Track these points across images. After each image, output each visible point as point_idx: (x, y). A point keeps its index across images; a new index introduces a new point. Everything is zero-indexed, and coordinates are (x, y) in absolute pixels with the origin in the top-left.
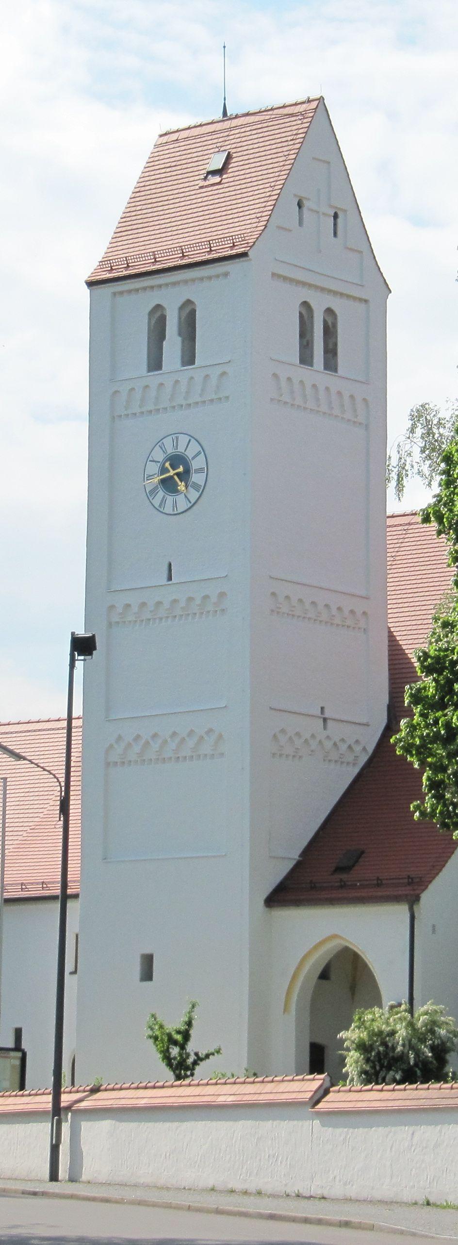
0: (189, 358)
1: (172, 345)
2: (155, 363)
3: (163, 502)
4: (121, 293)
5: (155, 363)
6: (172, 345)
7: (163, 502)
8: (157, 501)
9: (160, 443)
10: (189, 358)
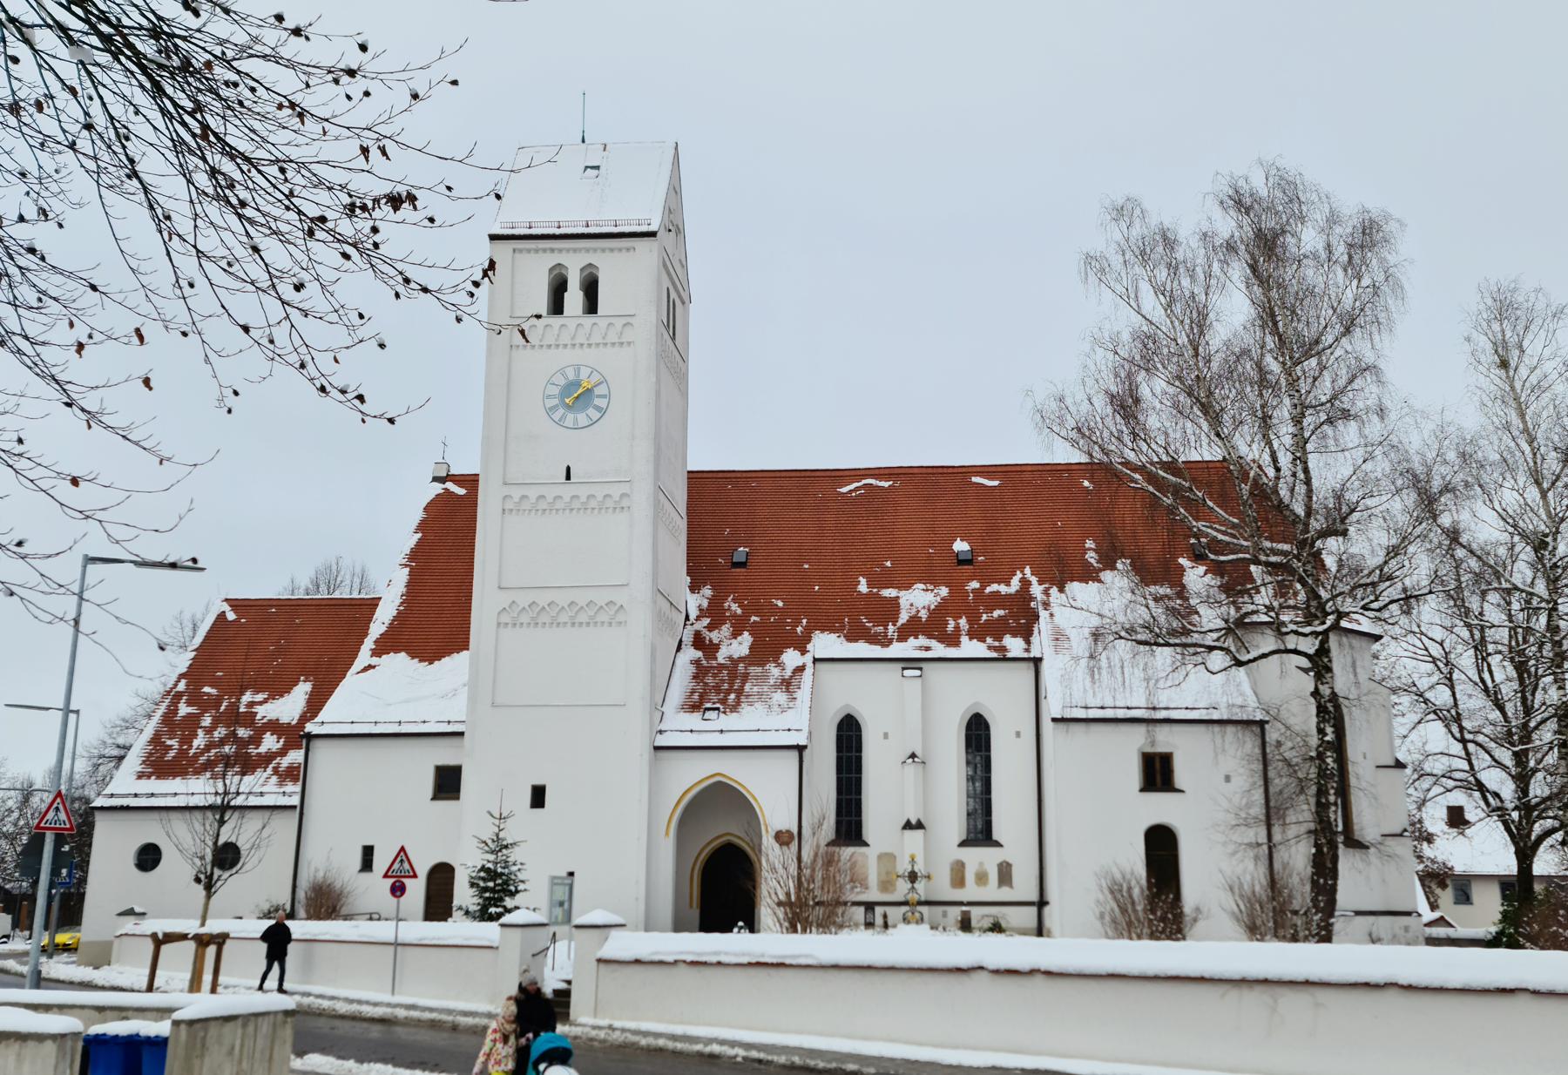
0: (591, 306)
1: (574, 298)
2: (557, 307)
3: (563, 418)
4: (521, 251)
5: (557, 307)
6: (574, 298)
7: (563, 418)
8: (557, 416)
9: (562, 371)
10: (591, 306)
